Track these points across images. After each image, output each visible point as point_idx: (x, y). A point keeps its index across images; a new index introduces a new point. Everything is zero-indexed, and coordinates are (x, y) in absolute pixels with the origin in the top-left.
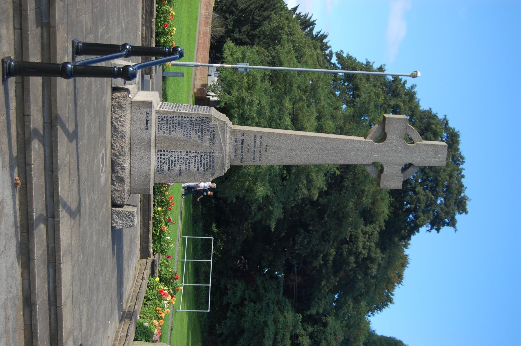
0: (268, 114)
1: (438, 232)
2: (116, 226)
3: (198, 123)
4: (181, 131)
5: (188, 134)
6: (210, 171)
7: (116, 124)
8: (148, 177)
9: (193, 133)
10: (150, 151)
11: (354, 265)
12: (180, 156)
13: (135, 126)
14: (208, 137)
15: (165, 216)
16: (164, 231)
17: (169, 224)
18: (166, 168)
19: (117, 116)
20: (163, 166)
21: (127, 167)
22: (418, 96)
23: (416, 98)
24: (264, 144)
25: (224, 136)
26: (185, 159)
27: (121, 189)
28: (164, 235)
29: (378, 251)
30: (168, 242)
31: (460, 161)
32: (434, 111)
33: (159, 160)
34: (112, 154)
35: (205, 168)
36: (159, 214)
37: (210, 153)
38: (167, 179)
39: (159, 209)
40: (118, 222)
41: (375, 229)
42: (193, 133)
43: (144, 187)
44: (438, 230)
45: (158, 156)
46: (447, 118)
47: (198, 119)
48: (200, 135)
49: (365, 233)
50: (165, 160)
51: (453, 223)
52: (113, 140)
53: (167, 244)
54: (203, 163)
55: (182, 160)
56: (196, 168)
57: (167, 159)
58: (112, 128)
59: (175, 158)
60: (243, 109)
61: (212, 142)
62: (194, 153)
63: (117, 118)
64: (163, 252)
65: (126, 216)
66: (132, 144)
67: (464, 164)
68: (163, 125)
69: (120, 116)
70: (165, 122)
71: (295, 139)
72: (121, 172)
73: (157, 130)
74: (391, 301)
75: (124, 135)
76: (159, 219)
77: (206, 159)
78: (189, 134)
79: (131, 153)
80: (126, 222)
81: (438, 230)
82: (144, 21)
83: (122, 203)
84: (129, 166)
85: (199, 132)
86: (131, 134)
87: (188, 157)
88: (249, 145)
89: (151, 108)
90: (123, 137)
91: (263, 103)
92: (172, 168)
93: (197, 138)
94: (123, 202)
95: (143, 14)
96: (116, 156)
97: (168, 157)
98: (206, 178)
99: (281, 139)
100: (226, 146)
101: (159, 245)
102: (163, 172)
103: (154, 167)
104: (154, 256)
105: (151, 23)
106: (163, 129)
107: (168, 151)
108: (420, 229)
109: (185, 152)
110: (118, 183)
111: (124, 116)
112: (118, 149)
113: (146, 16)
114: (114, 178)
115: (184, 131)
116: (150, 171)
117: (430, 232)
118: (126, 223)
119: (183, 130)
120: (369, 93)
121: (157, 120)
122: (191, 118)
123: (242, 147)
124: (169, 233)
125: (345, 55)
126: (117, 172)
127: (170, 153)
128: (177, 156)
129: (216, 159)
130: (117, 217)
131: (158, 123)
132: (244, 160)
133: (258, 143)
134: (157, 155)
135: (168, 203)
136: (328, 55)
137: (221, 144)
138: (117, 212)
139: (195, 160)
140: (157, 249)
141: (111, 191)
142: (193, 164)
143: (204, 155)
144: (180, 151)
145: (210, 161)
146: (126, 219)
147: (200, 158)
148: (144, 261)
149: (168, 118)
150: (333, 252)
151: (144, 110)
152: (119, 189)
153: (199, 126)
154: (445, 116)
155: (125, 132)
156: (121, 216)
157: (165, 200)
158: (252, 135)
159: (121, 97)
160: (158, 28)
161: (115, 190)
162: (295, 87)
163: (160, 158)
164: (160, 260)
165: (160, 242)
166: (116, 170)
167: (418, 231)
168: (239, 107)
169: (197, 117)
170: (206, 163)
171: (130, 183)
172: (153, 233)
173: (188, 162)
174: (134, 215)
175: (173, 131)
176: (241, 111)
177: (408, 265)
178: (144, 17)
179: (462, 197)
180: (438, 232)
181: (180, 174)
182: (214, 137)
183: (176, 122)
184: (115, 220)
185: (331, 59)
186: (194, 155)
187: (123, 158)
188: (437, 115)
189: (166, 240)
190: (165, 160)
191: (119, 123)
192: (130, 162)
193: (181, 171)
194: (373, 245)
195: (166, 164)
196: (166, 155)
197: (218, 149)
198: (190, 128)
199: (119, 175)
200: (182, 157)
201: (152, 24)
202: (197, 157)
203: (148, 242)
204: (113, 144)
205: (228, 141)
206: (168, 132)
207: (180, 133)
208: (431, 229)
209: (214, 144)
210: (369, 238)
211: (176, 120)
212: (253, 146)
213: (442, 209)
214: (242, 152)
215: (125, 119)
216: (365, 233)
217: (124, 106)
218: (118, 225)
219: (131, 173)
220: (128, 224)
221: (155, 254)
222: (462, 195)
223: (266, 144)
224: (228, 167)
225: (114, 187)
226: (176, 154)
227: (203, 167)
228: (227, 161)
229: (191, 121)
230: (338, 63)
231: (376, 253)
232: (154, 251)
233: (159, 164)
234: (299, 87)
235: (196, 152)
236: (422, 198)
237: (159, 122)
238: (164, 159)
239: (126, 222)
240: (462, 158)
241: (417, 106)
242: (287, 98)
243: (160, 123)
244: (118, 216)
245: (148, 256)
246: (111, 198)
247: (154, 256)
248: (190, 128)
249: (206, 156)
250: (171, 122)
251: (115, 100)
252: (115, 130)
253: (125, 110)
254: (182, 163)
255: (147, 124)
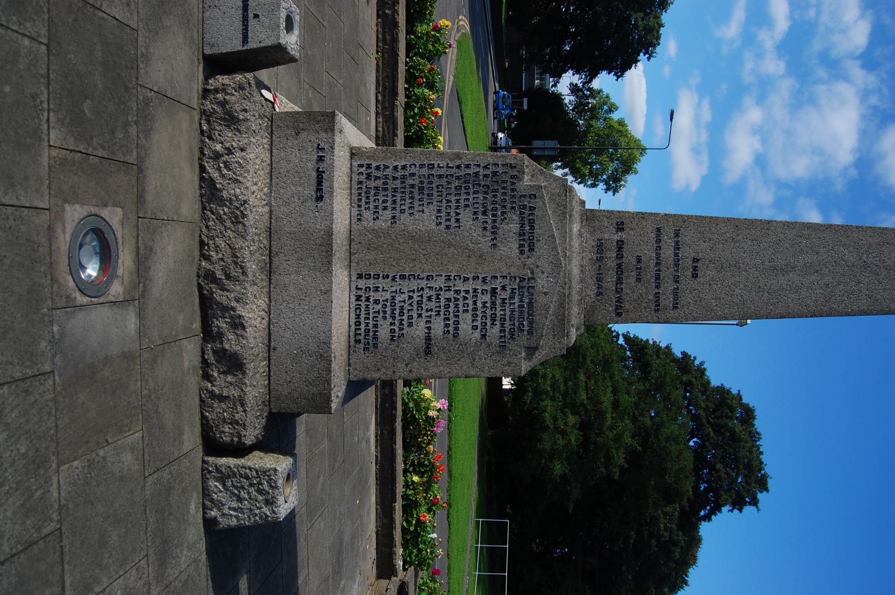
0: (562, 388)
1: (741, 512)
2: (220, 519)
3: (482, 183)
4: (430, 211)
5: (449, 220)
6: (523, 340)
7: (215, 175)
8: (324, 357)
9: (466, 216)
10: (329, 271)
11: (656, 549)
12: (427, 293)
13: (282, 191)
14: (514, 227)
15: (427, 493)
16: (425, 523)
17: (434, 508)
18: (384, 332)
19: (218, 147)
20: (375, 326)
21: (256, 323)
22: (708, 373)
23: (705, 375)
24: (687, 253)
25: (563, 227)
26: (443, 300)
27: (234, 392)
28: (424, 531)
29: (680, 533)
30: (432, 544)
31: (756, 437)
32: (727, 386)
33: (363, 305)
34: (202, 273)
35: (507, 330)
36: (414, 489)
37: (522, 280)
38: (387, 368)
39: (416, 479)
40: (223, 505)
41: (676, 509)
42: (466, 216)
43: (314, 390)
44: (740, 510)
45: (360, 293)
46: (741, 393)
47: (482, 172)
48: (490, 221)
49: (665, 514)
50: (380, 306)
51: (754, 502)
52: (207, 227)
53: (432, 547)
54: (499, 313)
55: (432, 305)
56: (479, 330)
57: (387, 300)
58: (201, 187)
59: (411, 298)
60: (536, 383)
61: (527, 243)
62: (471, 281)
63: (217, 156)
64: (421, 563)
65: (251, 485)
66: (274, 249)
67: (761, 440)
68: (372, 192)
69: (226, 148)
70: (379, 183)
71: (782, 236)
72: (231, 337)
73: (355, 211)
74: (686, 583)
75: (242, 212)
76: (414, 499)
77: (510, 298)
78: (453, 220)
79: (270, 280)
80: (249, 506)
81: (740, 510)
82: (380, 107)
83: (236, 439)
84: (265, 322)
85: (484, 213)
86: (271, 218)
87: (451, 295)
88: (639, 260)
89: (333, 130)
90: (238, 219)
91: (557, 376)
92: (401, 329)
93: (480, 231)
94: (239, 436)
95: (379, 92)
96: (214, 279)
97: (388, 296)
98: (509, 364)
99: (740, 237)
100: (570, 261)
101: (414, 551)
102: (375, 346)
103: (346, 327)
104: (405, 573)
105: (394, 108)
106: (372, 207)
107: (388, 276)
108: (723, 508)
109: (443, 278)
110: (225, 373)
111: (242, 150)
112: (220, 256)
113: (384, 96)
114: (210, 357)
115: (439, 211)
116: (330, 337)
117: (732, 512)
118: (251, 510)
119: (434, 207)
120: (664, 366)
121: (355, 177)
122: (459, 167)
123: (619, 266)
124: (434, 527)
125: (632, 336)
126: (220, 335)
127: (394, 283)
128: (418, 291)
129: (541, 300)
130: (220, 487)
131: (359, 188)
132: (627, 305)
133: (668, 252)
134: (357, 288)
135: (433, 466)
136: (614, 337)
137: (555, 249)
138: (221, 472)
139: (475, 303)
140: (411, 558)
141: (201, 400)
142: (469, 316)
143: (504, 288)
144: (426, 274)
145: (522, 306)
146: (249, 493)
147: (489, 295)
148: (384, 583)
149: (389, 172)
150: (633, 534)
151: (309, 138)
152: (225, 394)
153: (486, 193)
154: (739, 391)
155: (245, 202)
156: (233, 485)
157: (426, 462)
158: (650, 228)
159: (233, 85)
160: (408, 126)
161: (213, 395)
162: (588, 361)
163: (363, 299)
164: (419, 579)
165: (416, 545)
166: (215, 329)
167: (720, 511)
168: (532, 381)
169: (479, 166)
170: (508, 313)
171: (269, 376)
172: (403, 526)
173: (451, 310)
174: (275, 482)
175: (403, 211)
176: (535, 385)
177: (701, 546)
178: (380, 98)
179: (762, 475)
180: (741, 512)
181: (428, 351)
182: (532, 228)
183: (411, 182)
184: (215, 496)
185: (618, 340)
186: (470, 286)
187: (238, 288)
188: (731, 390)
189: (429, 539)
190: (379, 307)
191: (225, 171)
192: (270, 310)
193: (430, 339)
194: (674, 526)
195: (385, 318)
196: (383, 290)
197: (547, 268)
198: (458, 201)
199: (227, 346)
200: (433, 293)
201: (395, 110)
202: (479, 295)
203: (391, 544)
204: (206, 240)
205: (576, 243)
206: (388, 214)
207: (425, 216)
208: (733, 509)
209: (533, 250)
210: (669, 519)
211: (413, 174)
212: (652, 264)
213: (743, 487)
214: (619, 281)
215: (243, 158)
216: (665, 514)
217: (241, 117)
218: (224, 515)
219: (273, 344)
220: (257, 512)
221: (407, 569)
222: (763, 472)
223: (692, 255)
224: (578, 329)
225: (209, 385)
226: (414, 284)
227: (498, 325)
228: (575, 310)
229: (458, 178)
230: (625, 344)
231: (678, 536)
232: (405, 562)
233: (362, 320)
234: (592, 361)
235: (476, 278)
236: (724, 476)
237: (360, 183)
238: (376, 302)
239: (249, 506)
240: (758, 434)
241: (708, 382)
242: (581, 371)
243: (364, 187)
244: (224, 486)
245: (393, 574)
246: (202, 425)
247: (405, 573)
248: (458, 201)
249: (509, 291)
250: (398, 183)
251: (212, 96)
252: (212, 194)
253: (243, 128)
254: (434, 313)
255: (320, 182)
